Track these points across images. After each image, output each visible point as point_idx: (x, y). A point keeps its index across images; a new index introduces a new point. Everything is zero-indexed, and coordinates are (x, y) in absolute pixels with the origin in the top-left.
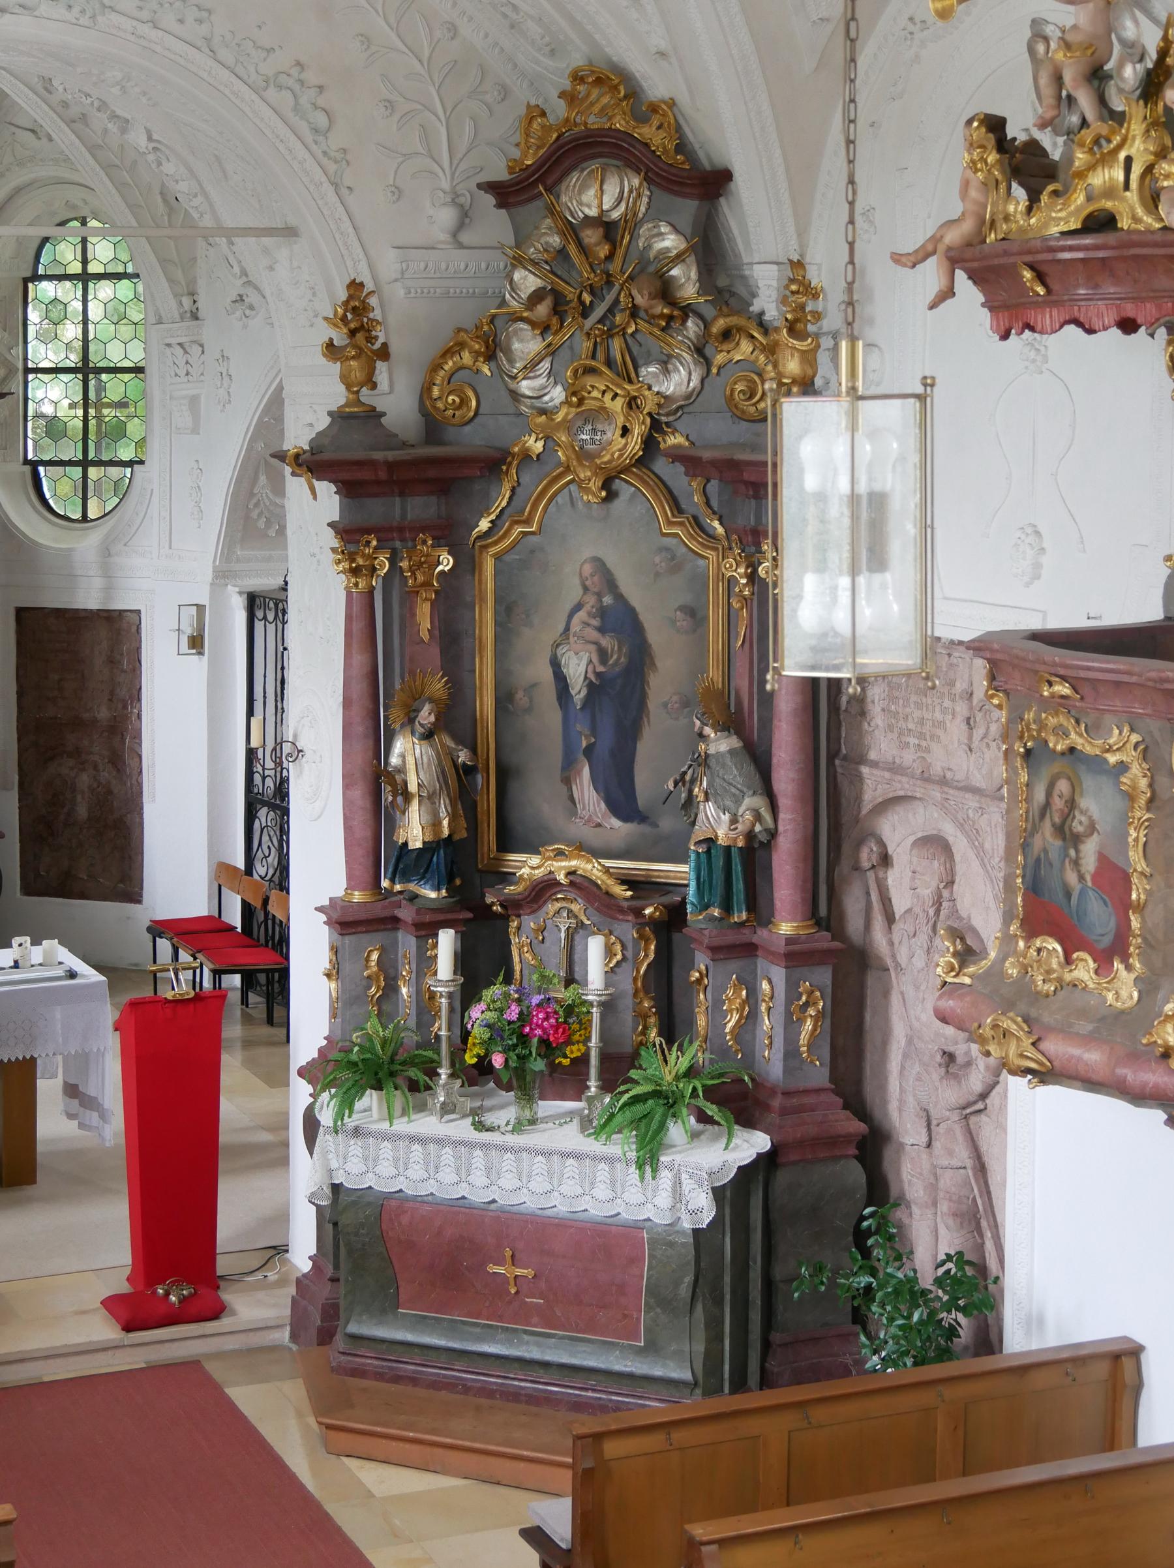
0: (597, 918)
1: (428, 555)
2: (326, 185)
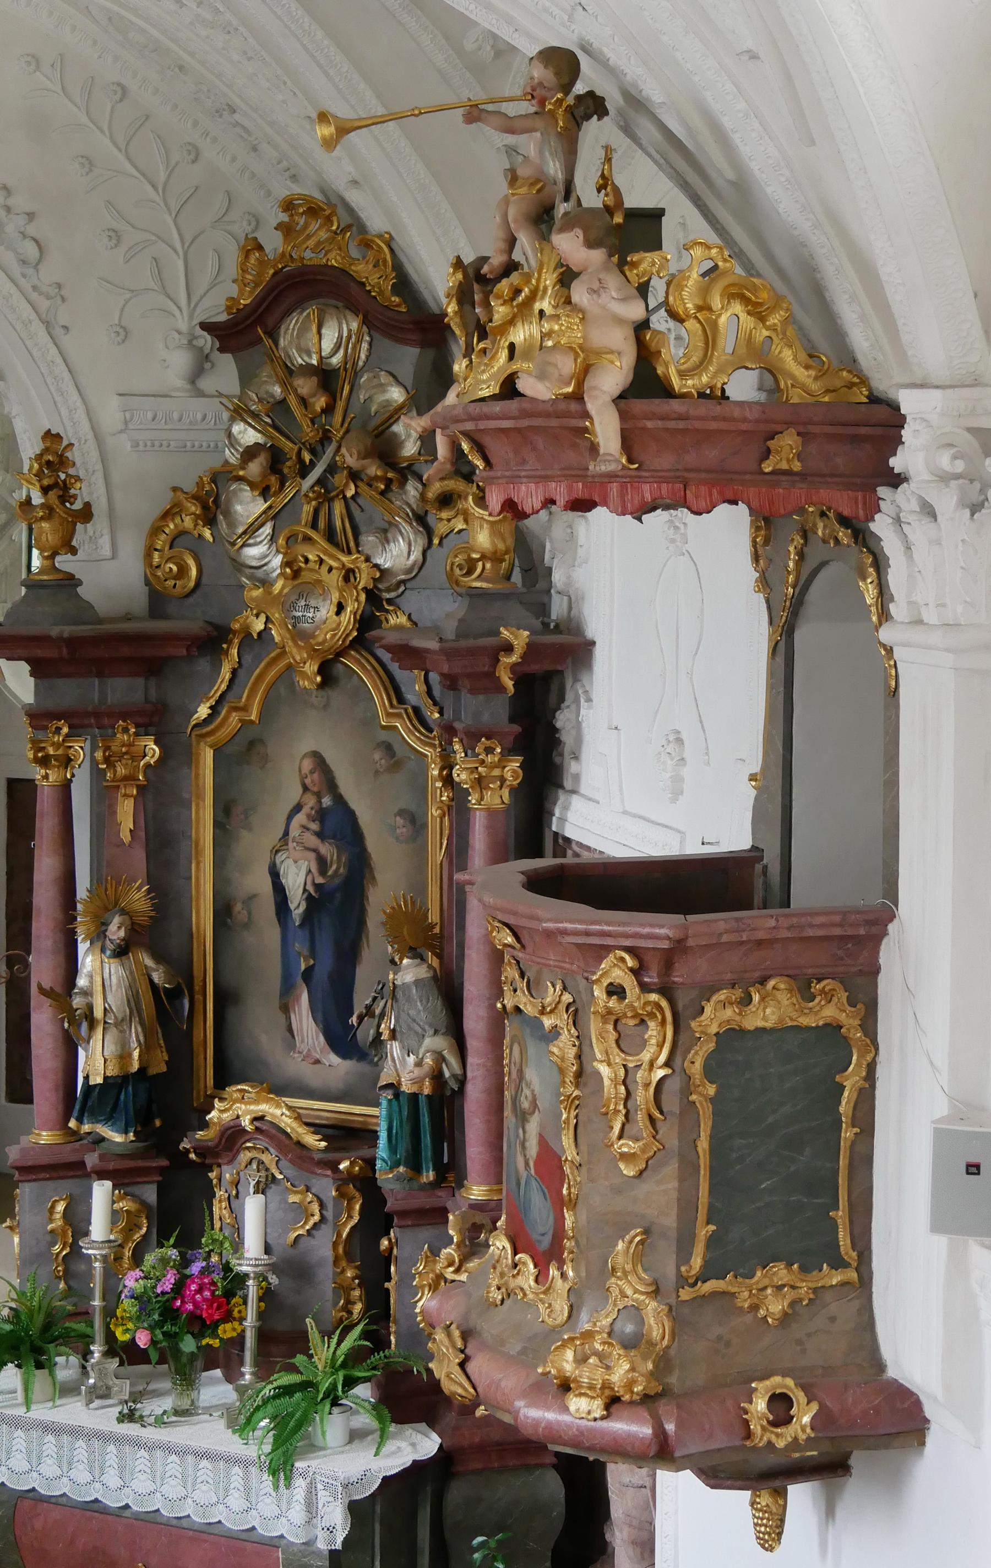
0: (291, 1171)
1: (130, 745)
2: (37, 322)
